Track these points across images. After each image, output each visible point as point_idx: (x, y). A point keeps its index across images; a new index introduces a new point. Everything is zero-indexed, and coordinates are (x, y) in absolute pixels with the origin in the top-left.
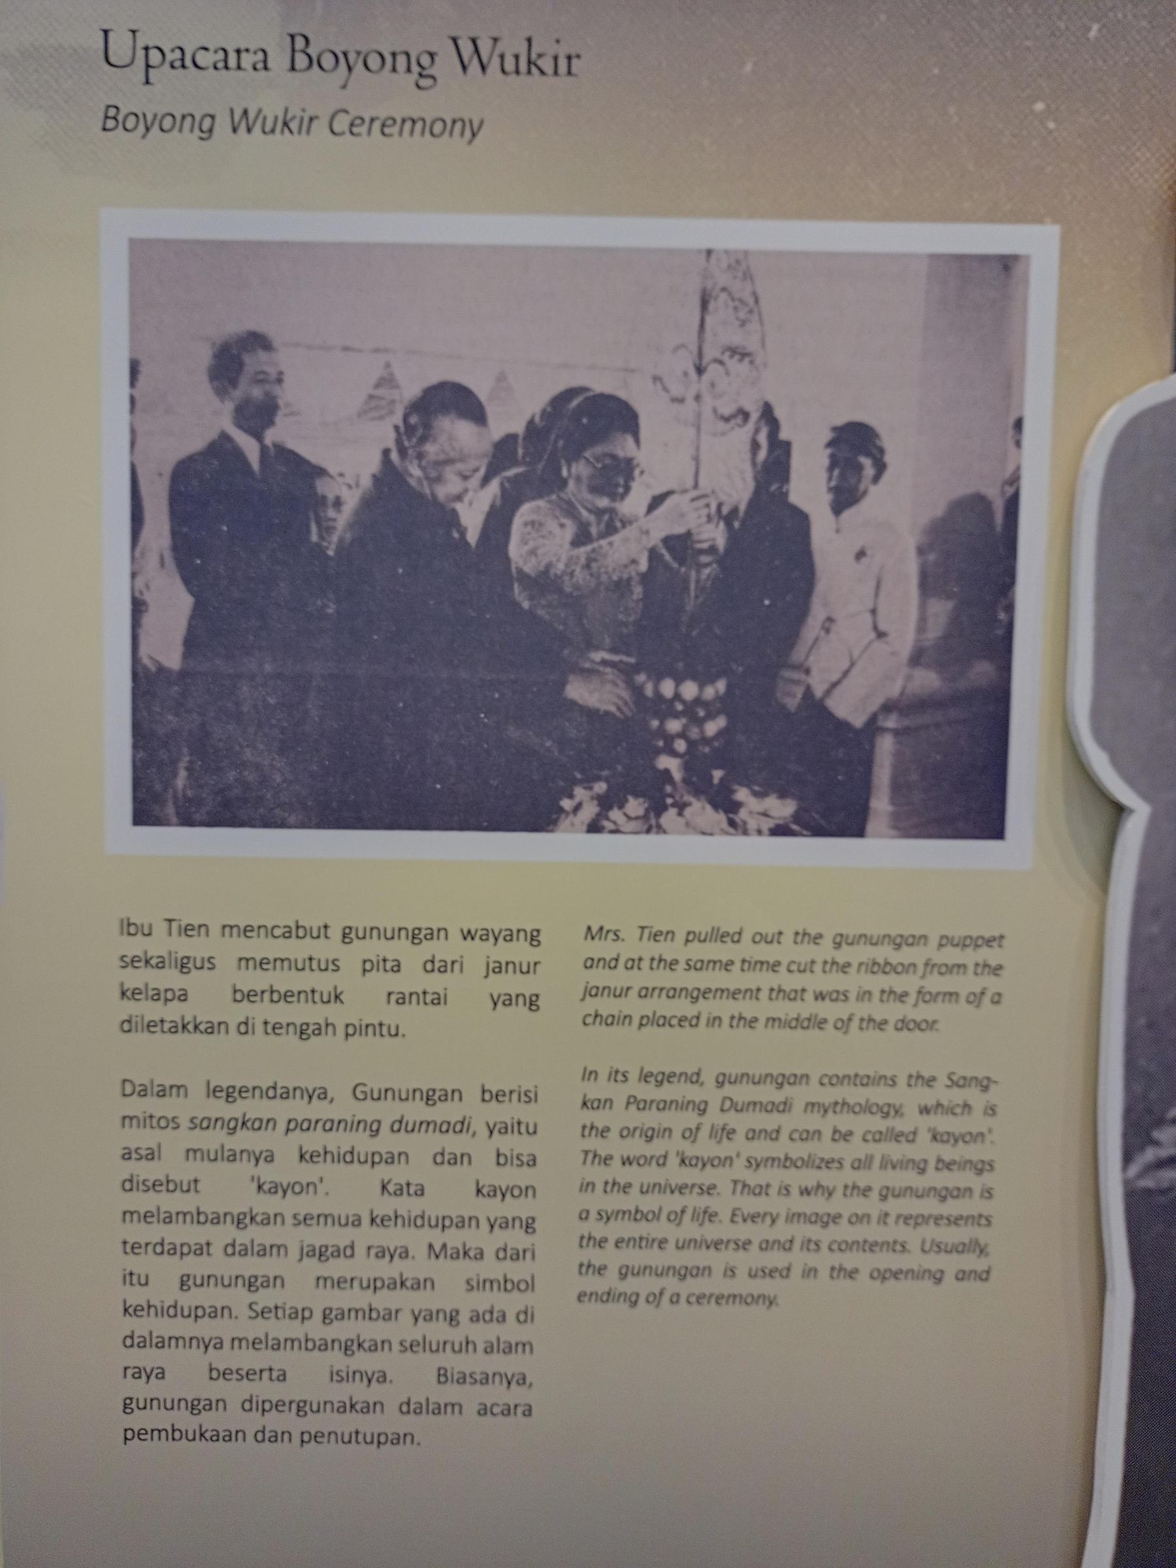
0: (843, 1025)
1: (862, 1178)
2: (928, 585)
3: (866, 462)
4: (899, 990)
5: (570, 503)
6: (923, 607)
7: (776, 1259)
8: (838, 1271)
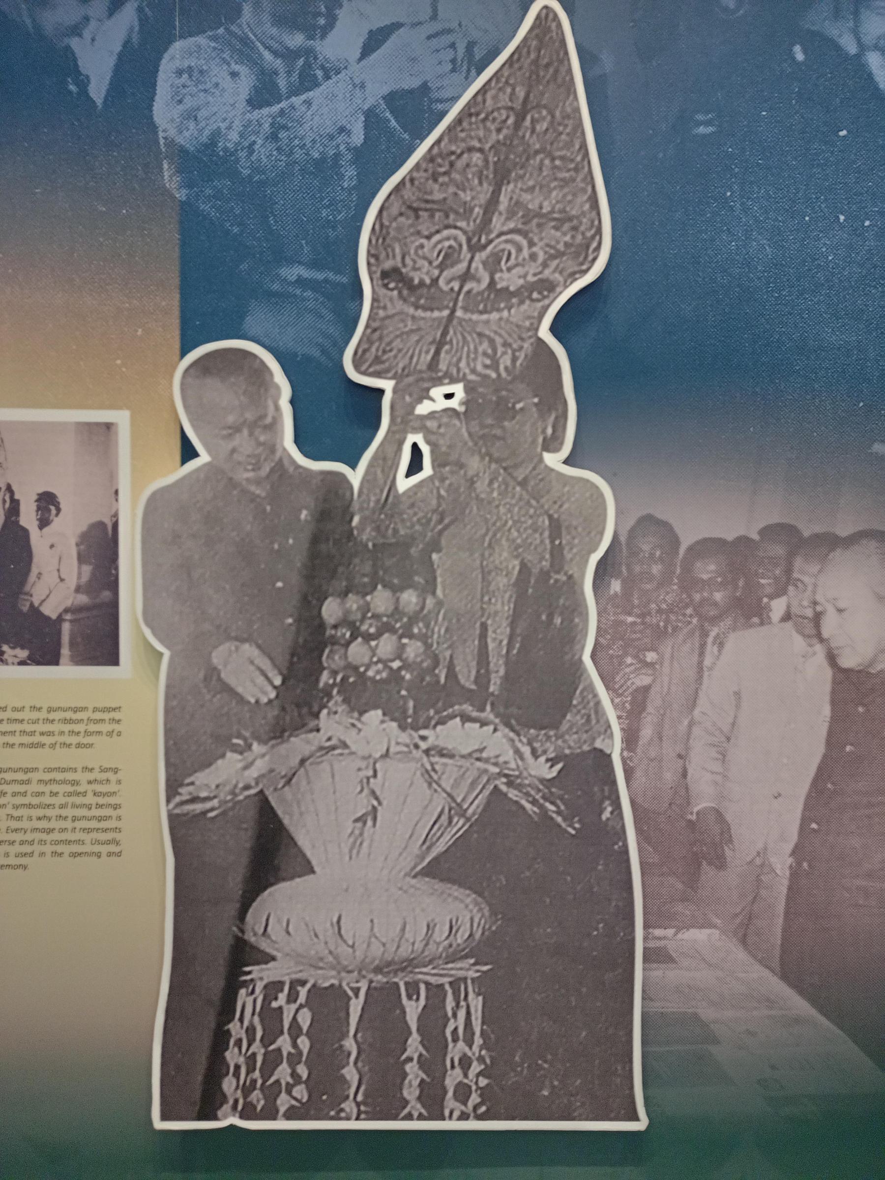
0: (53, 746)
1: (64, 812)
2: (81, 559)
3: (52, 508)
5: (245, 41)
6: (79, 568)
7: (27, 849)
8: (55, 854)
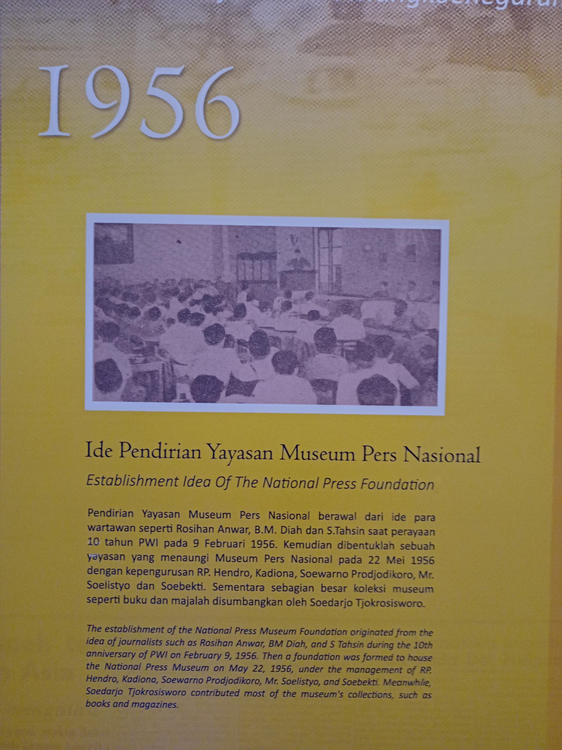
4: (406, 643)
8: (287, 693)
